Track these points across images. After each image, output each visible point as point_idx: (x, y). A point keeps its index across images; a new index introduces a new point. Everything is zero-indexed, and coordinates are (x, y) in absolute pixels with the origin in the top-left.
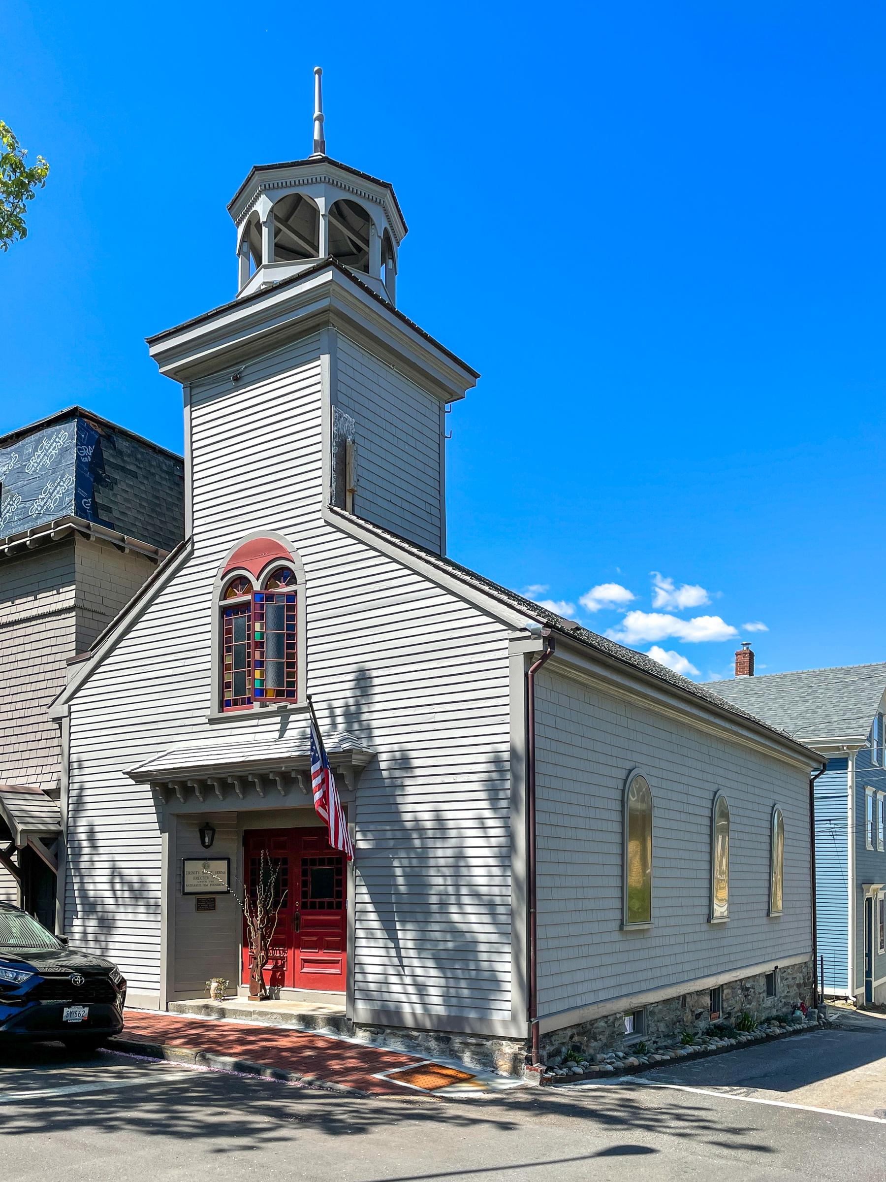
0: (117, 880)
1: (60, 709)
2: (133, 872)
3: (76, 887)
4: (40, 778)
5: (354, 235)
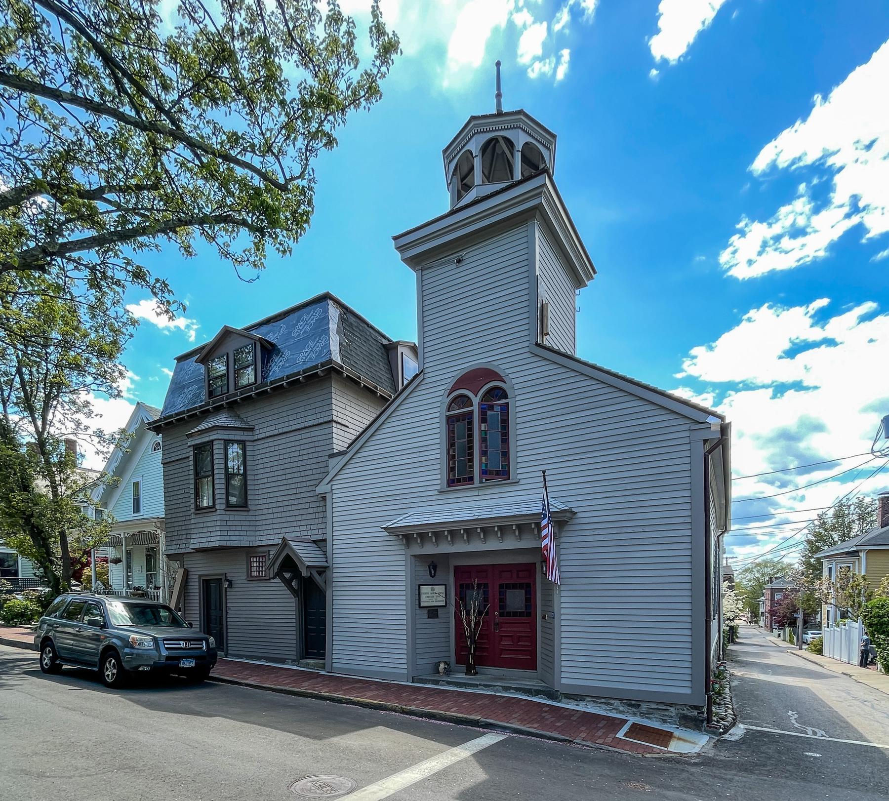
1: (321, 489)
4: (310, 533)
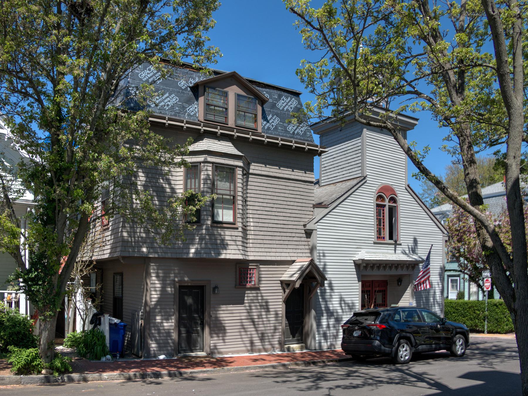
0: (343, 302)
2: (349, 299)
3: (323, 306)
5: (413, 112)
